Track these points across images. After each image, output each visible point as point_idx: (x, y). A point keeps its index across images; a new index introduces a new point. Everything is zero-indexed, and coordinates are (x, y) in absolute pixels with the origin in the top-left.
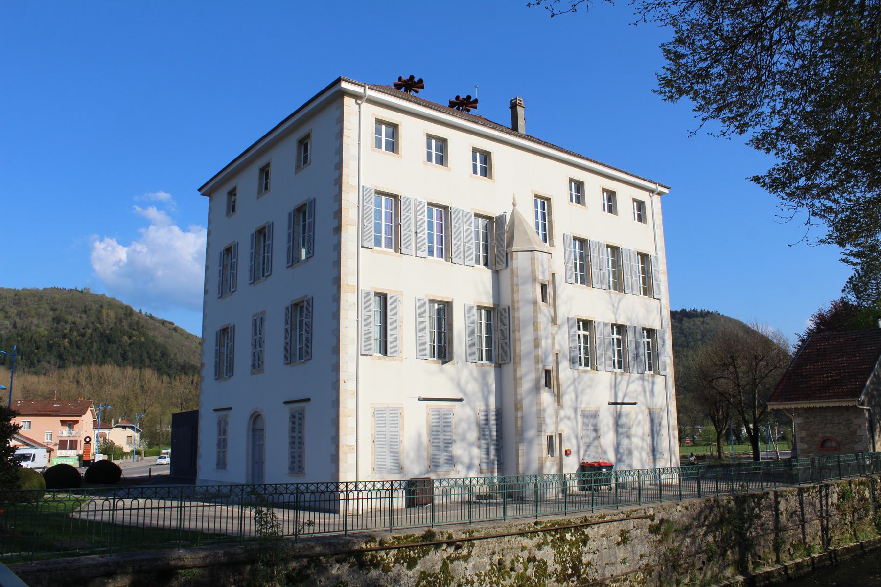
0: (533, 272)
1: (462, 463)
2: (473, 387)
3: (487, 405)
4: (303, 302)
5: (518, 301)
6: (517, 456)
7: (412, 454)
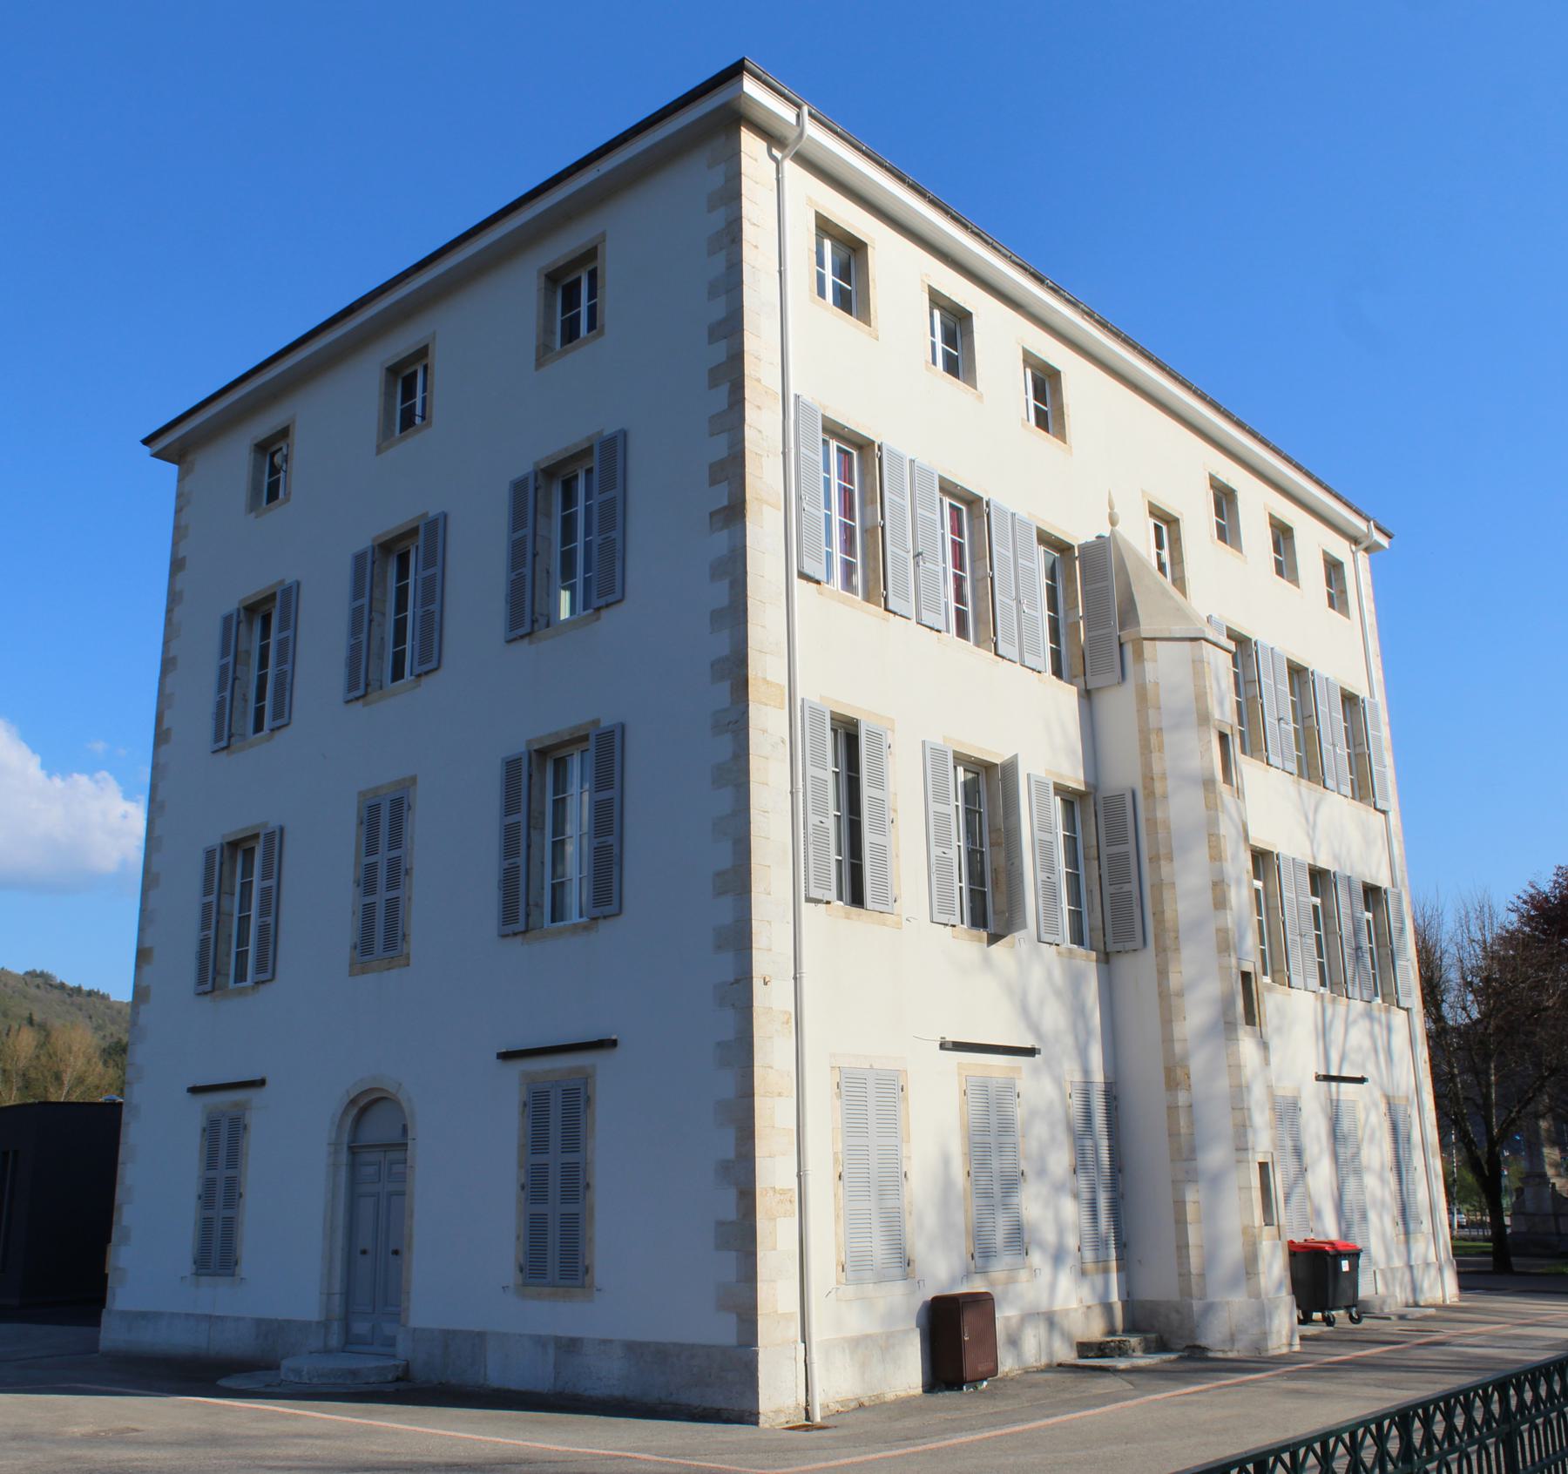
0: (1201, 696)
1: (1041, 1245)
2: (1054, 1017)
3: (1086, 1072)
4: (256, 836)
5: (1164, 777)
6: (1181, 1222)
7: (931, 1220)
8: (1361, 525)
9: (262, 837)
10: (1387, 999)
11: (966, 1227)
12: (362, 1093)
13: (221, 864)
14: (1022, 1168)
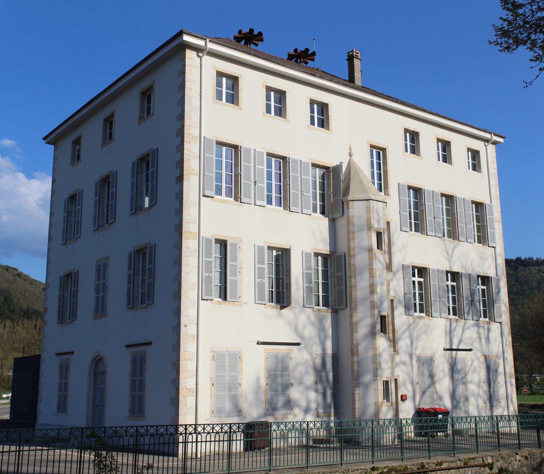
1: (299, 407)
2: (310, 332)
3: (324, 350)
5: (354, 249)
6: (354, 401)
7: (250, 398)
8: (488, 136)
9: (148, 248)
10: (491, 319)
11: (265, 401)
12: (96, 356)
13: (64, 282)
14: (291, 382)
